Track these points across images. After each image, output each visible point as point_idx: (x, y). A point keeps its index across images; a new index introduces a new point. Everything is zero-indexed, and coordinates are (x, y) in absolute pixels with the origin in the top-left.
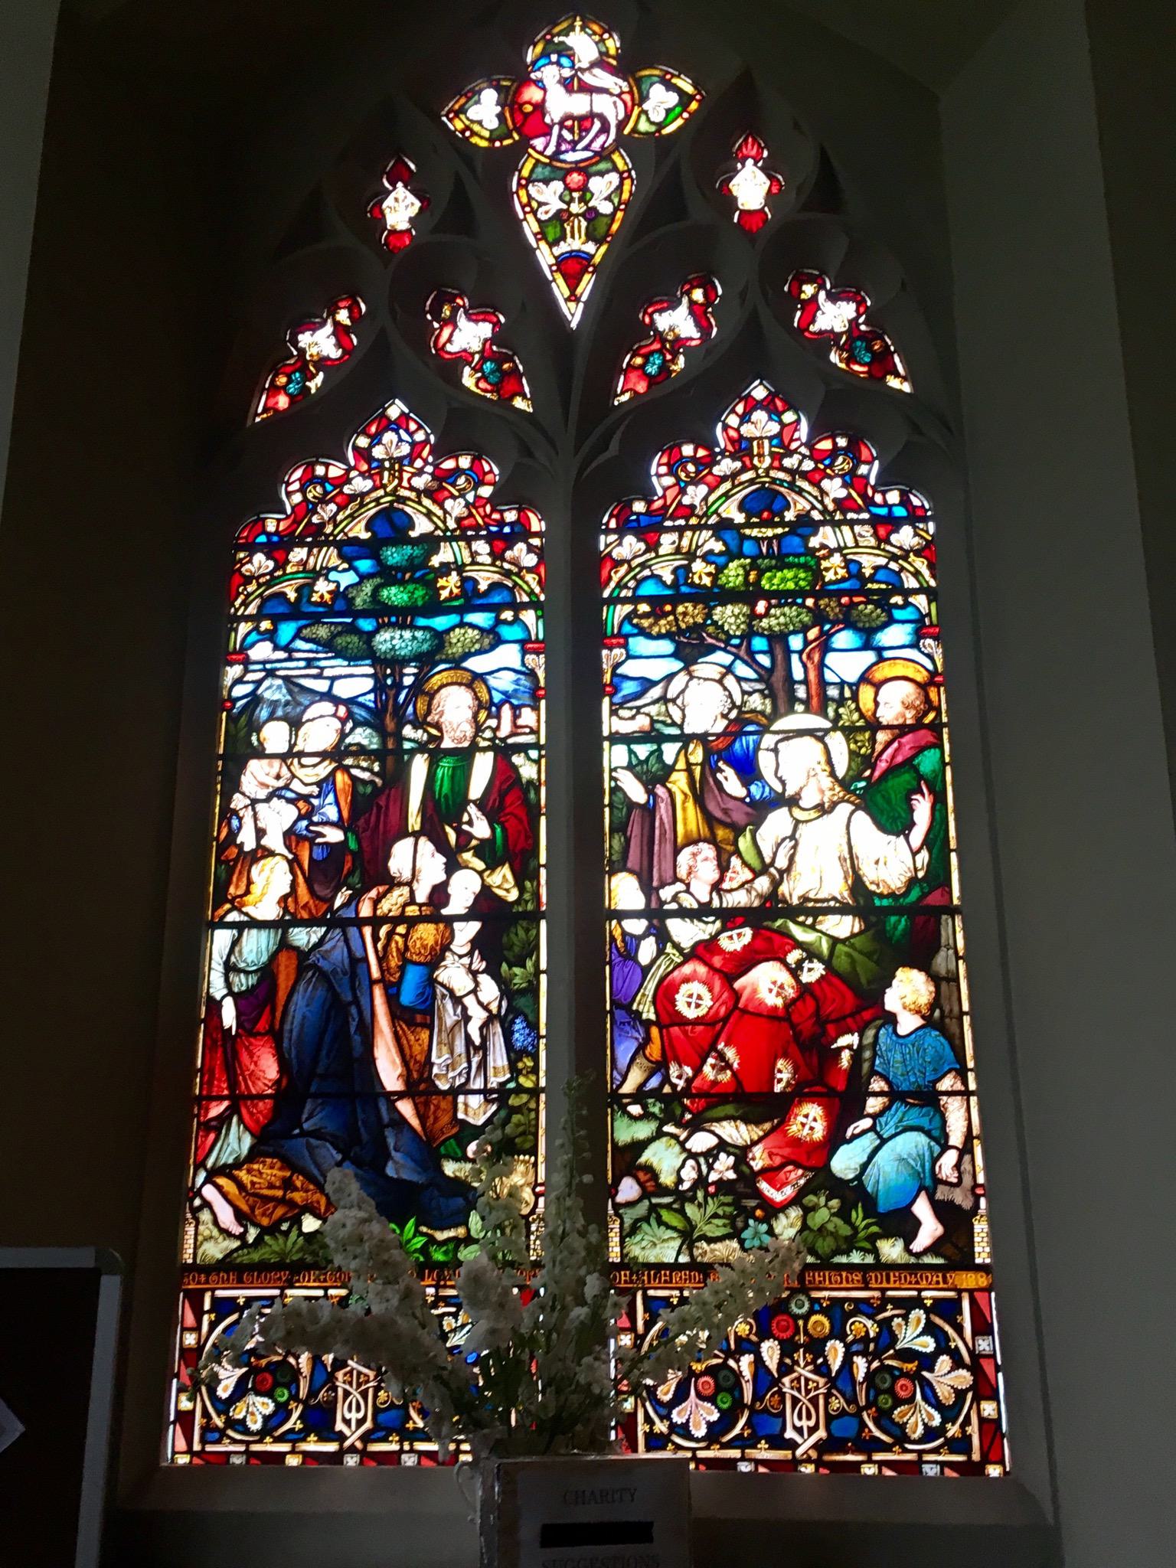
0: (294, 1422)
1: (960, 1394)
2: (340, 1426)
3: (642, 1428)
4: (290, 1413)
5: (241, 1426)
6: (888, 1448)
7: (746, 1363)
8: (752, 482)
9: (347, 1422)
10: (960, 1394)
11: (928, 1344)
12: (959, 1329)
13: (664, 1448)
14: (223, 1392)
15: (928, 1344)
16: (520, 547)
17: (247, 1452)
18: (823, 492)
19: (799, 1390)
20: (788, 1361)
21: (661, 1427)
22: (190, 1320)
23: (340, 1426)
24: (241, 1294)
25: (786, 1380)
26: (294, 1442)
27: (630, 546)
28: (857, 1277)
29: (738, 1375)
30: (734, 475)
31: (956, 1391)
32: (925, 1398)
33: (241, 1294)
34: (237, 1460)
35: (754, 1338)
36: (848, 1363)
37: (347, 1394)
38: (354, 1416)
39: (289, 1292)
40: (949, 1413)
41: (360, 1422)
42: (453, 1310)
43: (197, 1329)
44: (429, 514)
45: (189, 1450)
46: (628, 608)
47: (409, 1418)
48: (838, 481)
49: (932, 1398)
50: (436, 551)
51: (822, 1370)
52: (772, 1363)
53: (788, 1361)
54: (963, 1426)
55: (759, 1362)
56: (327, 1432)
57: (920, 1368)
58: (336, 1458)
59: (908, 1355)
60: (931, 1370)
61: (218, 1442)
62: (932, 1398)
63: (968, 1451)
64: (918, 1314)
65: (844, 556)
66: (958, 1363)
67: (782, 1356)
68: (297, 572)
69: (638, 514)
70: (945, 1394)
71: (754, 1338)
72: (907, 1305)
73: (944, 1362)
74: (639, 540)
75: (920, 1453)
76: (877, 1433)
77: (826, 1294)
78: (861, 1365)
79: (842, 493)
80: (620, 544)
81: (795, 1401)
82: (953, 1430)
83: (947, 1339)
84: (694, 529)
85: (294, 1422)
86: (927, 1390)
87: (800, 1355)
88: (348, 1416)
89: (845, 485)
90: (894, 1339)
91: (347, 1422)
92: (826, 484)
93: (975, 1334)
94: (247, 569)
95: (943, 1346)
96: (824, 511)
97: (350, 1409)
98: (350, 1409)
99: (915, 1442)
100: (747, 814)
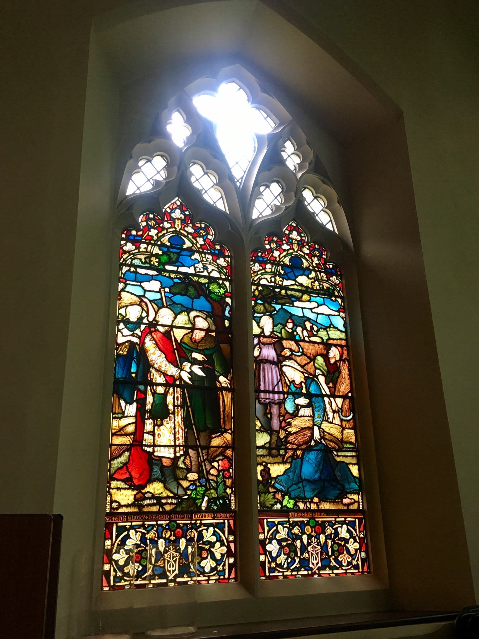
0: (296, 564)
1: (223, 555)
2: (311, 565)
3: (267, 566)
4: (295, 561)
5: (128, 575)
6: (337, 569)
7: (298, 543)
8: (173, 232)
9: (313, 564)
10: (356, 550)
11: (213, 539)
12: (355, 530)
13: (274, 572)
14: (121, 563)
15: (213, 539)
16: (222, 259)
17: (283, 575)
18: (197, 242)
19: (170, 558)
20: (167, 549)
21: (273, 565)
22: (261, 530)
23: (311, 565)
24: (276, 520)
25: (166, 555)
26: (150, 580)
27: (129, 247)
28: (125, 517)
29: (296, 547)
30: (288, 250)
31: (355, 549)
32: (347, 553)
33: (276, 520)
34: (281, 578)
35: (300, 534)
36: (326, 542)
37: (168, 562)
38: (315, 562)
39: (146, 523)
40: (218, 562)
41: (317, 564)
42: (206, 528)
43: (264, 533)
44: (307, 260)
45: (109, 585)
46: (127, 268)
47: (331, 562)
48: (201, 239)
49: (213, 557)
50: (193, 254)
51: (319, 544)
52: (305, 542)
53: (167, 549)
54: (357, 561)
55: (302, 542)
56: (163, 575)
57: (210, 547)
58: (166, 584)
59: (209, 543)
60: (348, 544)
61: (120, 582)
62: (213, 557)
63: (358, 569)
64: (345, 526)
65: (203, 264)
66: (222, 545)
67: (308, 539)
68: (144, 252)
69: (134, 235)
70: (218, 557)
71: (300, 534)
72: (208, 526)
73: (218, 544)
74: (133, 245)
75: (346, 570)
76: (335, 564)
77: (320, 519)
78: (330, 542)
79: (203, 243)
80: (254, 266)
81: (168, 562)
82: (220, 568)
83: (353, 534)
84: (152, 244)
85: (296, 564)
86: (212, 555)
87: (313, 539)
88: (169, 569)
89: (318, 260)
90: (203, 537)
91: (313, 564)
92: (198, 239)
93: (228, 535)
94: (125, 248)
95: (351, 537)
96: (313, 267)
97: (170, 567)
98: (170, 567)
99: (345, 566)
100: (274, 358)
